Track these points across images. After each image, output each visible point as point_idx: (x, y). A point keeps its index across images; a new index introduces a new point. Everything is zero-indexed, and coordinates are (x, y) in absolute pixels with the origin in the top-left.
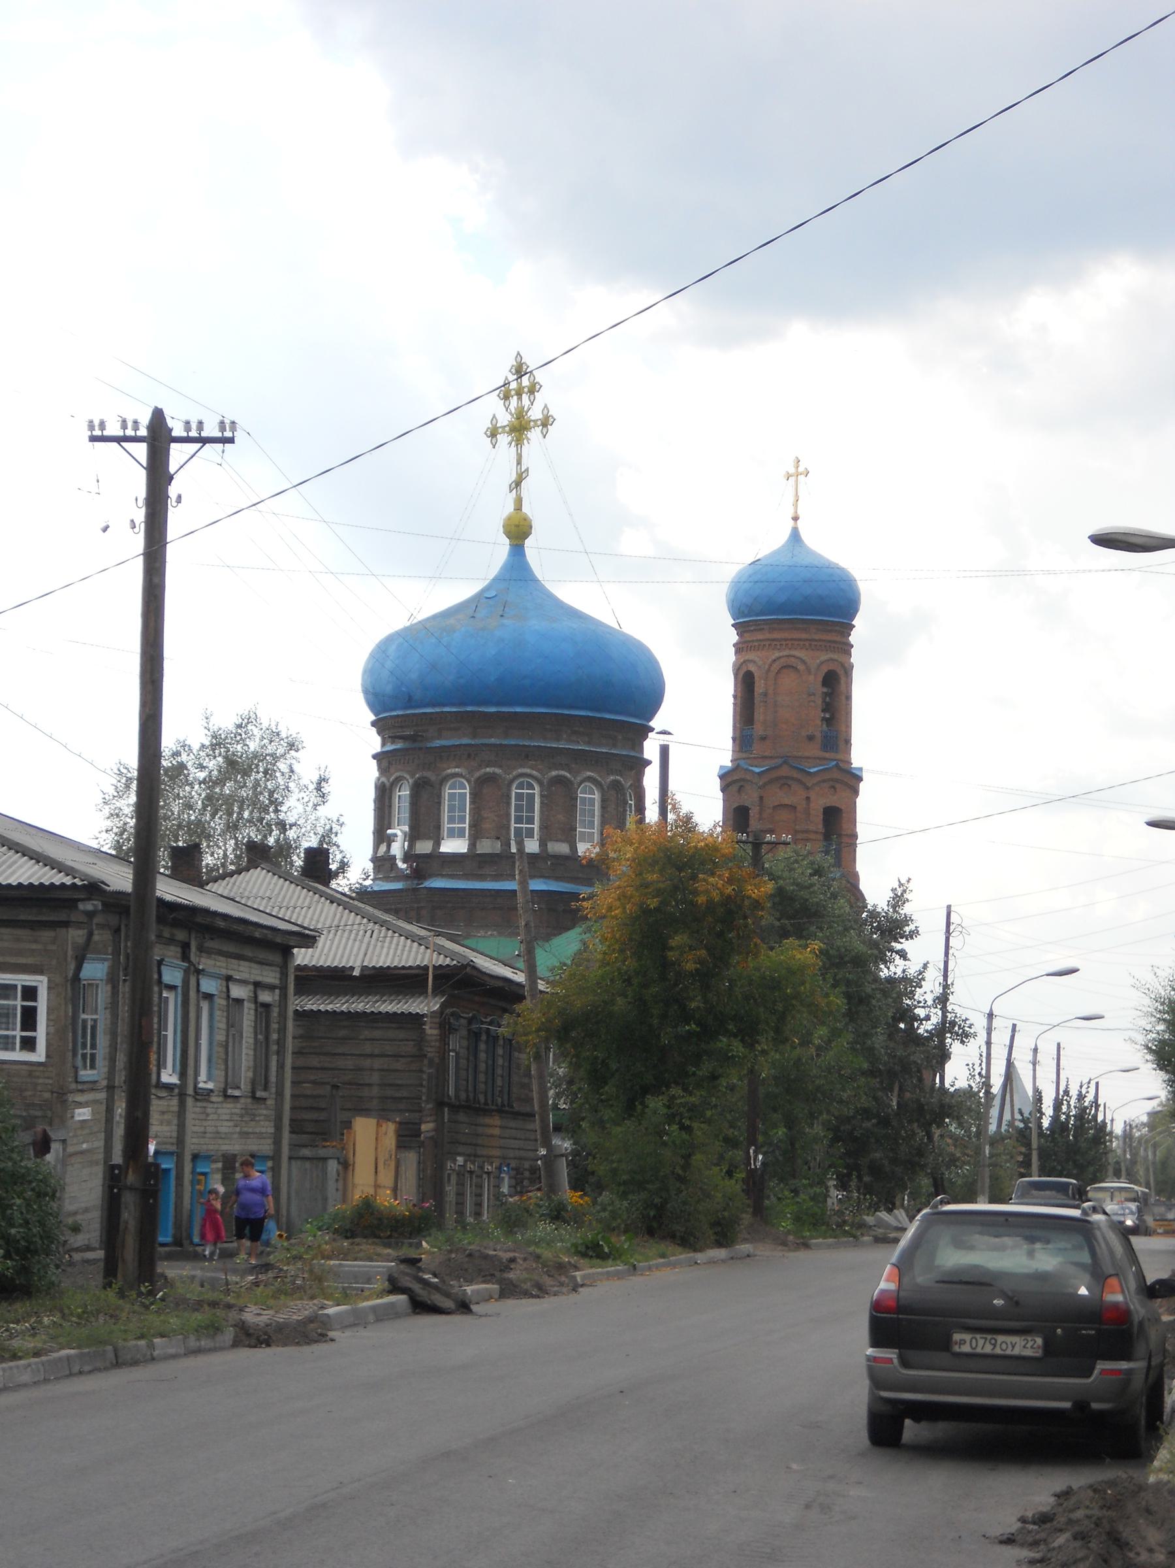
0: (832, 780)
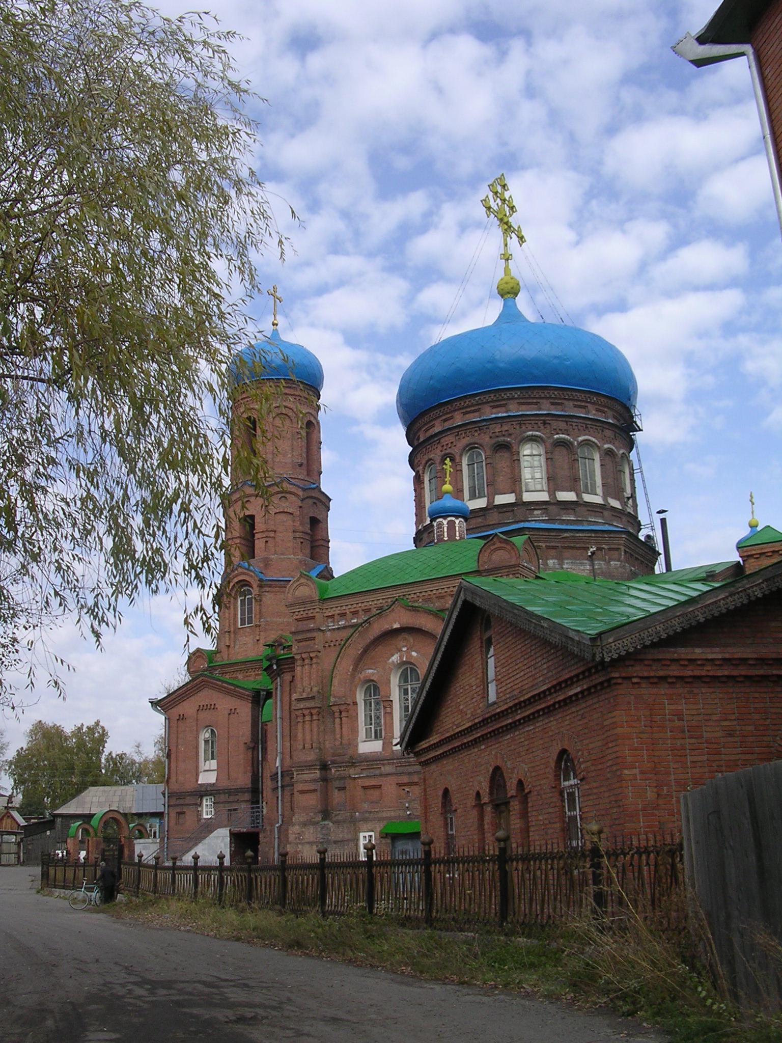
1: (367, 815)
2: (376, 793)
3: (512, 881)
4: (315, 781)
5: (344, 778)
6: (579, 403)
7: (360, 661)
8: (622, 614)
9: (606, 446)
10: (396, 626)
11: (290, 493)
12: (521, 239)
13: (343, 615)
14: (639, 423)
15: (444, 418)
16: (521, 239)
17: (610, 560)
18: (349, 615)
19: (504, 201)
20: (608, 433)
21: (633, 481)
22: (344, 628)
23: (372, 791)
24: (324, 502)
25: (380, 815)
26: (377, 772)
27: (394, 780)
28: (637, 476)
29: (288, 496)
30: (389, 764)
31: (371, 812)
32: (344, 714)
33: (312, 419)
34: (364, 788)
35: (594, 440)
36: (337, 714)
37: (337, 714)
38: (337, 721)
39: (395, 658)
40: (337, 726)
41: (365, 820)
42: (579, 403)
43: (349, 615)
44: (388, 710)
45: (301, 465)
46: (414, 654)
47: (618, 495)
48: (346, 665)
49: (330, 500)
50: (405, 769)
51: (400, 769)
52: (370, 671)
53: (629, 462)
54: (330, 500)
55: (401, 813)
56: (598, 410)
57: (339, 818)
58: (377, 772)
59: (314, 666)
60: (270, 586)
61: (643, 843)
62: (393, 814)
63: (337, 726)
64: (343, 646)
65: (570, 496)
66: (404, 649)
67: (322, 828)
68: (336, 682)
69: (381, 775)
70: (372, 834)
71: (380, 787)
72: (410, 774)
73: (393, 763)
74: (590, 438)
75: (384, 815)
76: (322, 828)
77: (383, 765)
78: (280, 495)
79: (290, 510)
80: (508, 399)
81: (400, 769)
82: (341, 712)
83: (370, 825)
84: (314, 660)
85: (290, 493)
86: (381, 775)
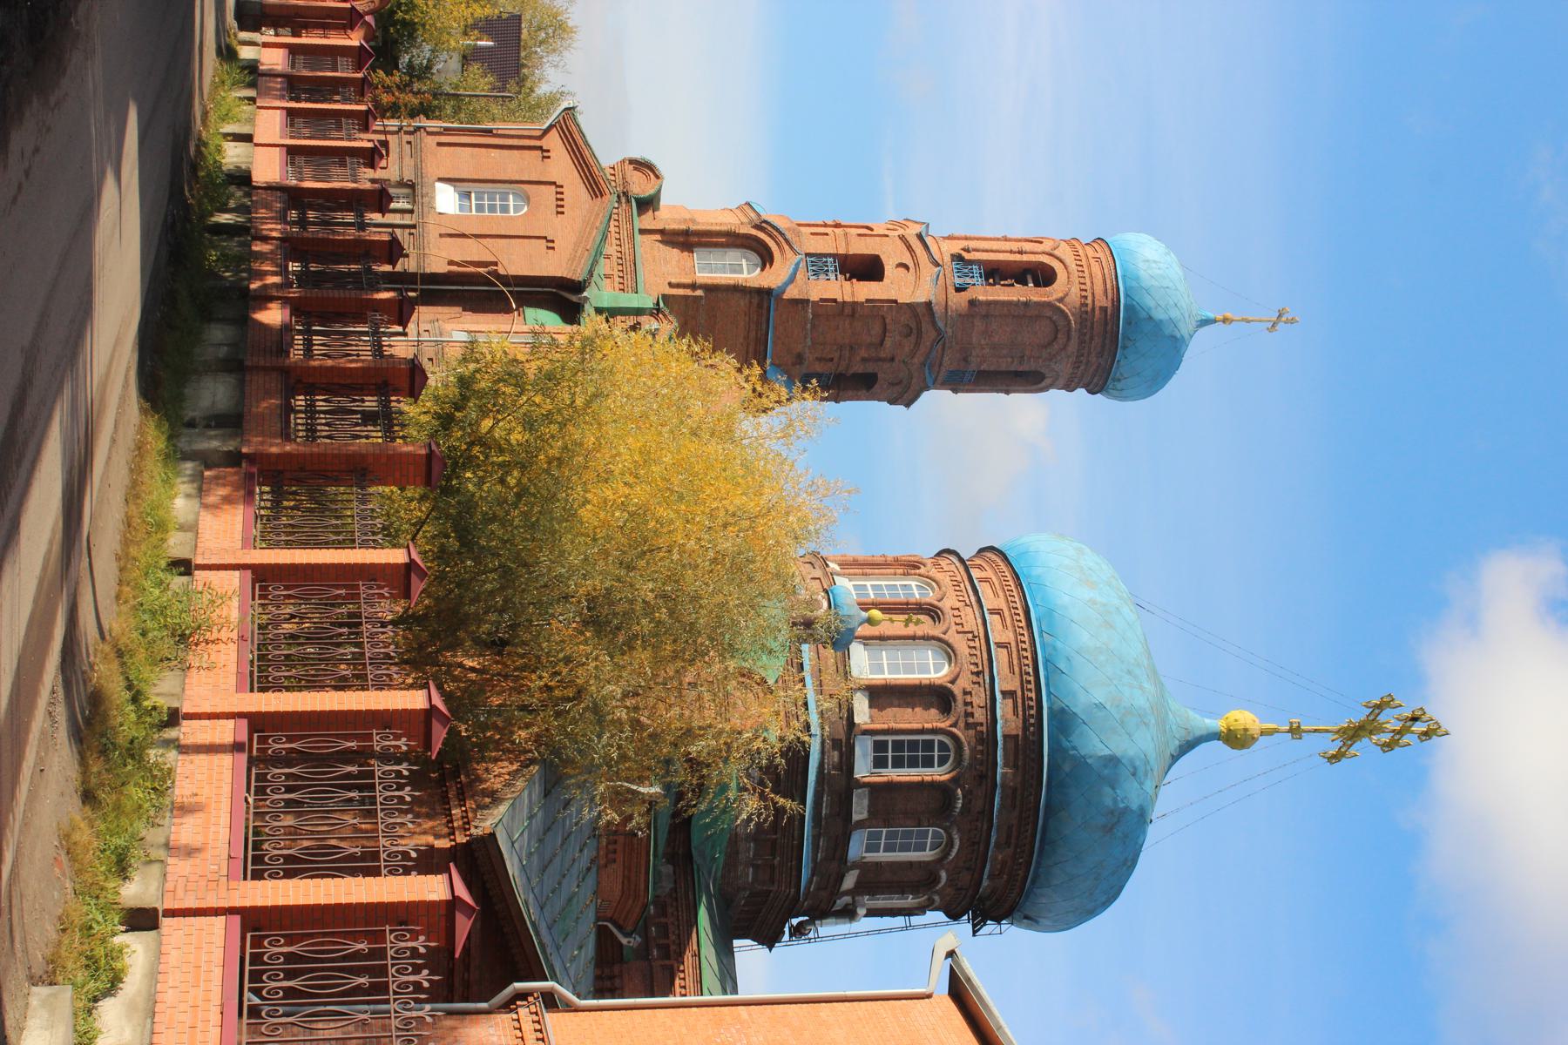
0: (917, 265)
3: (907, 779)
6: (1014, 834)
8: (123, 399)
9: (943, 875)
11: (917, 344)
12: (1335, 758)
14: (985, 930)
15: (1007, 613)
16: (1335, 758)
17: (756, 867)
19: (1400, 733)
20: (965, 878)
21: (893, 912)
24: (904, 395)
28: (900, 921)
29: (913, 339)
33: (1047, 381)
35: (953, 854)
42: (1014, 834)
45: (965, 360)
47: (863, 887)
49: (908, 405)
53: (920, 910)
54: (908, 405)
56: (1004, 863)
60: (760, 306)
65: (860, 810)
74: (955, 850)
78: (913, 325)
79: (888, 342)
80: (1025, 720)
85: (917, 344)
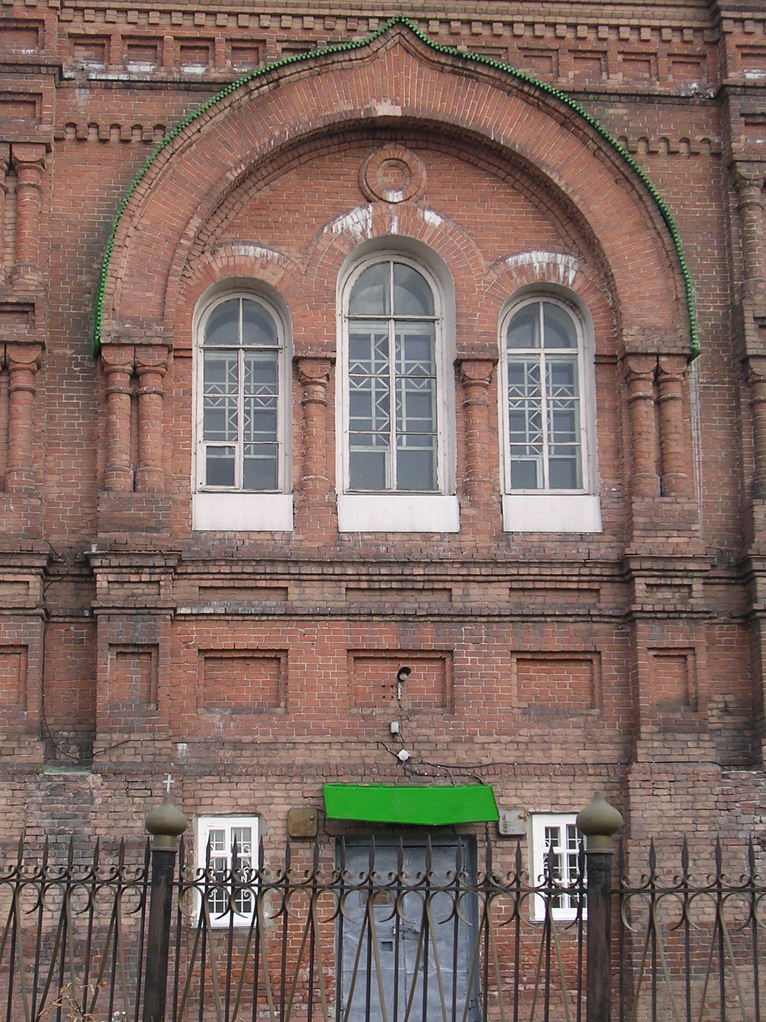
1: (227, 754)
2: (261, 676)
4: (21, 612)
5: (151, 611)
7: (232, 201)
10: (385, 109)
13: (144, 44)
18: (171, 51)
22: (152, 86)
23: (236, 670)
25: (283, 757)
26: (272, 602)
27: (343, 635)
30: (323, 578)
31: (238, 745)
32: (151, 382)
34: (209, 655)
36: (121, 380)
37: (121, 380)
38: (122, 403)
39: (357, 221)
40: (121, 423)
41: (226, 773)
43: (171, 51)
44: (319, 392)
46: (432, 218)
48: (163, 210)
50: (389, 602)
51: (371, 602)
52: (254, 251)
55: (372, 754)
57: (127, 756)
58: (272, 602)
59: (28, 196)
61: (382, 911)
62: (335, 755)
63: (121, 423)
64: (148, 144)
66: (395, 197)
67: (54, 791)
68: (121, 264)
69: (289, 615)
70: (252, 823)
71: (276, 657)
72: (406, 618)
73: (338, 579)
75: (299, 757)
76: (54, 791)
77: (299, 579)
81: (371, 602)
82: (135, 376)
83: (244, 792)
84: (30, 176)
86: (289, 615)
